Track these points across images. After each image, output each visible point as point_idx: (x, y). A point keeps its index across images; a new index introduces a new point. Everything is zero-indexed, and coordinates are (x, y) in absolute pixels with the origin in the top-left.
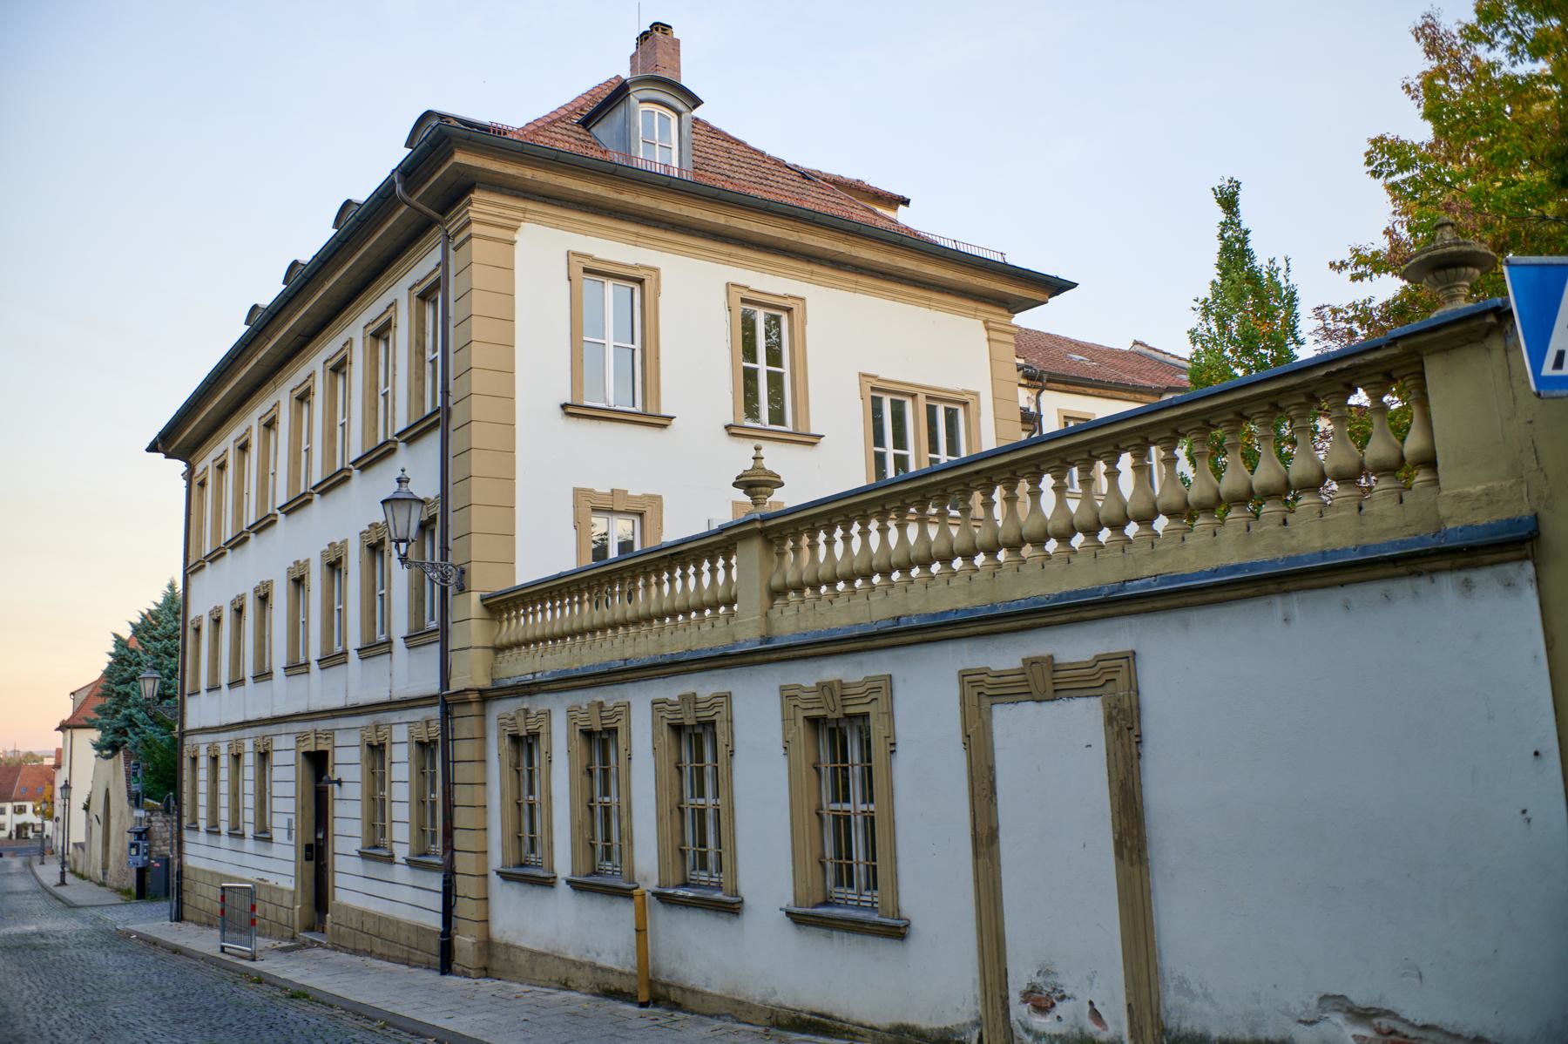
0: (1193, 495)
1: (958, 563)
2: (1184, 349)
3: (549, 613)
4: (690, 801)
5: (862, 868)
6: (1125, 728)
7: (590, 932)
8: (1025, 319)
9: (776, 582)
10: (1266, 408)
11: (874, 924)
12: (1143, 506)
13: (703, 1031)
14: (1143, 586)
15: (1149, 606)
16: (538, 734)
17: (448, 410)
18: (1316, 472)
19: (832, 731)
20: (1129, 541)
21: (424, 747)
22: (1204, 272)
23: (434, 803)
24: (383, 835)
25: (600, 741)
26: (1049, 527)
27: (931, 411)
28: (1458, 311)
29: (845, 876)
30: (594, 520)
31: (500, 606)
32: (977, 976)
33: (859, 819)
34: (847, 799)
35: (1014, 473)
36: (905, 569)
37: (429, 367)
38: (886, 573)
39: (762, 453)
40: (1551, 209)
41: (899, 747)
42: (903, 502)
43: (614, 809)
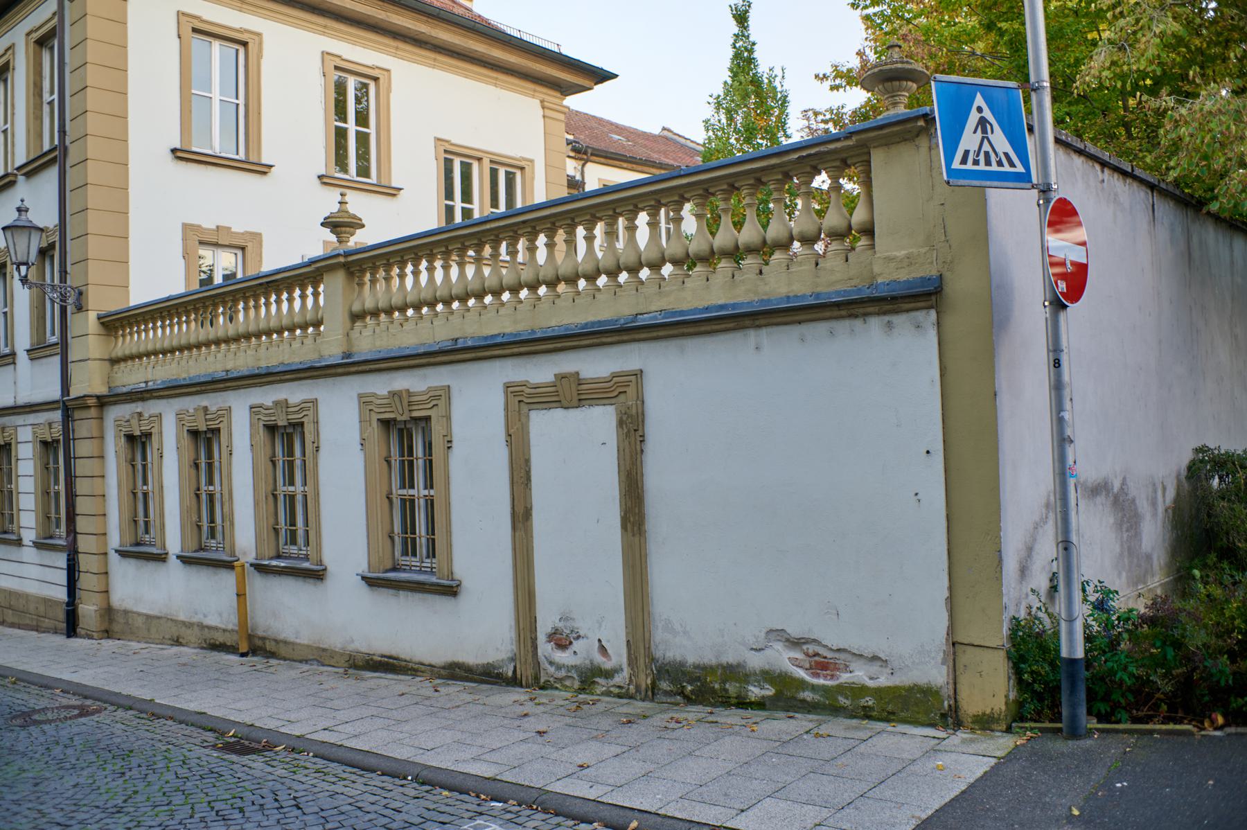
0: (693, 248)
1: (506, 296)
2: (698, 135)
3: (160, 331)
4: (282, 489)
5: (424, 540)
6: (632, 429)
7: (206, 599)
8: (575, 102)
9: (356, 307)
10: (752, 182)
11: (432, 584)
12: (654, 255)
13: (293, 673)
14: (651, 319)
15: (655, 334)
16: (150, 434)
17: (65, 149)
18: (786, 235)
19: (401, 431)
20: (642, 282)
21: (47, 446)
22: (718, 74)
23: (57, 494)
24: (12, 522)
25: (205, 439)
26: (580, 269)
27: (494, 173)
28: (898, 115)
29: (410, 548)
30: (202, 252)
31: (114, 324)
32: (513, 623)
33: (422, 501)
34: (412, 487)
35: (554, 224)
36: (463, 299)
37: (46, 108)
38: (447, 302)
39: (347, 199)
40: (980, 47)
41: (454, 444)
42: (463, 244)
43: (218, 496)
